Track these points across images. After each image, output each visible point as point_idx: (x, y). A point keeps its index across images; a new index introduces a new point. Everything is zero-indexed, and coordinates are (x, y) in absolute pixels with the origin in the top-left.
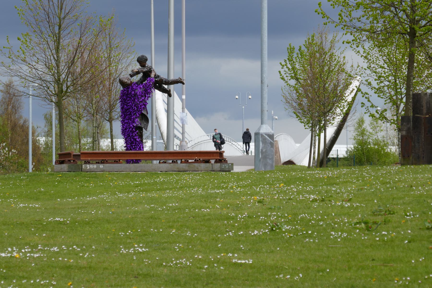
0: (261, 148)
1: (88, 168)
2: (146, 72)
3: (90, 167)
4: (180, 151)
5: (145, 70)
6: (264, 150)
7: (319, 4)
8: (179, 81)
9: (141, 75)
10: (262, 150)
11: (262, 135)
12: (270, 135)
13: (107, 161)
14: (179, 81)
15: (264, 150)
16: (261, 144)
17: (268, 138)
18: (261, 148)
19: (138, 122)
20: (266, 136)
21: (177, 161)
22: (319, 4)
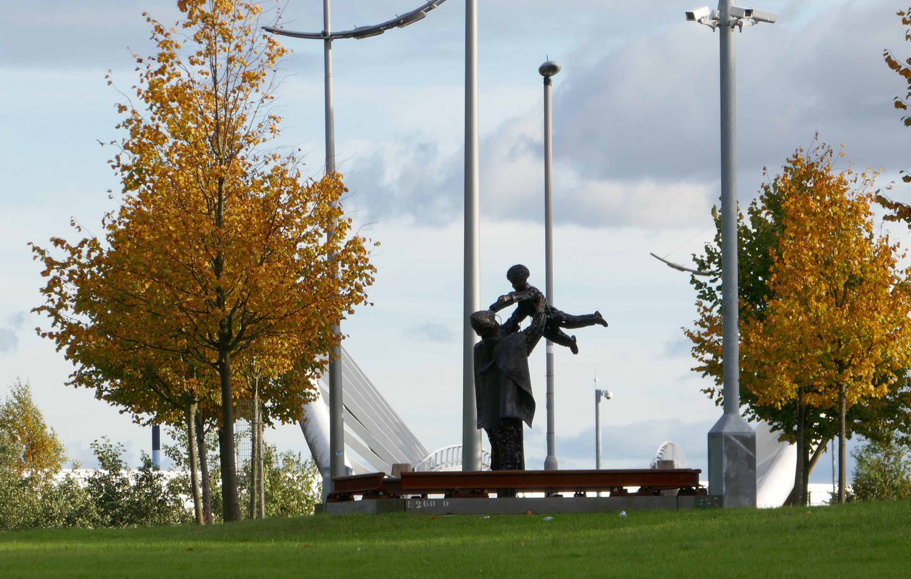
0: (724, 471)
1: (419, 507)
2: (528, 301)
3: (422, 505)
4: (661, 469)
5: (525, 297)
6: (732, 475)
7: (73, 224)
8: (595, 319)
9: (515, 306)
10: (727, 474)
11: (727, 439)
12: (747, 439)
13: (457, 492)
14: (595, 319)
15: (732, 475)
16: (725, 460)
17: (741, 445)
18: (724, 471)
19: (511, 409)
20: (738, 442)
21: (659, 491)
22: (73, 224)
